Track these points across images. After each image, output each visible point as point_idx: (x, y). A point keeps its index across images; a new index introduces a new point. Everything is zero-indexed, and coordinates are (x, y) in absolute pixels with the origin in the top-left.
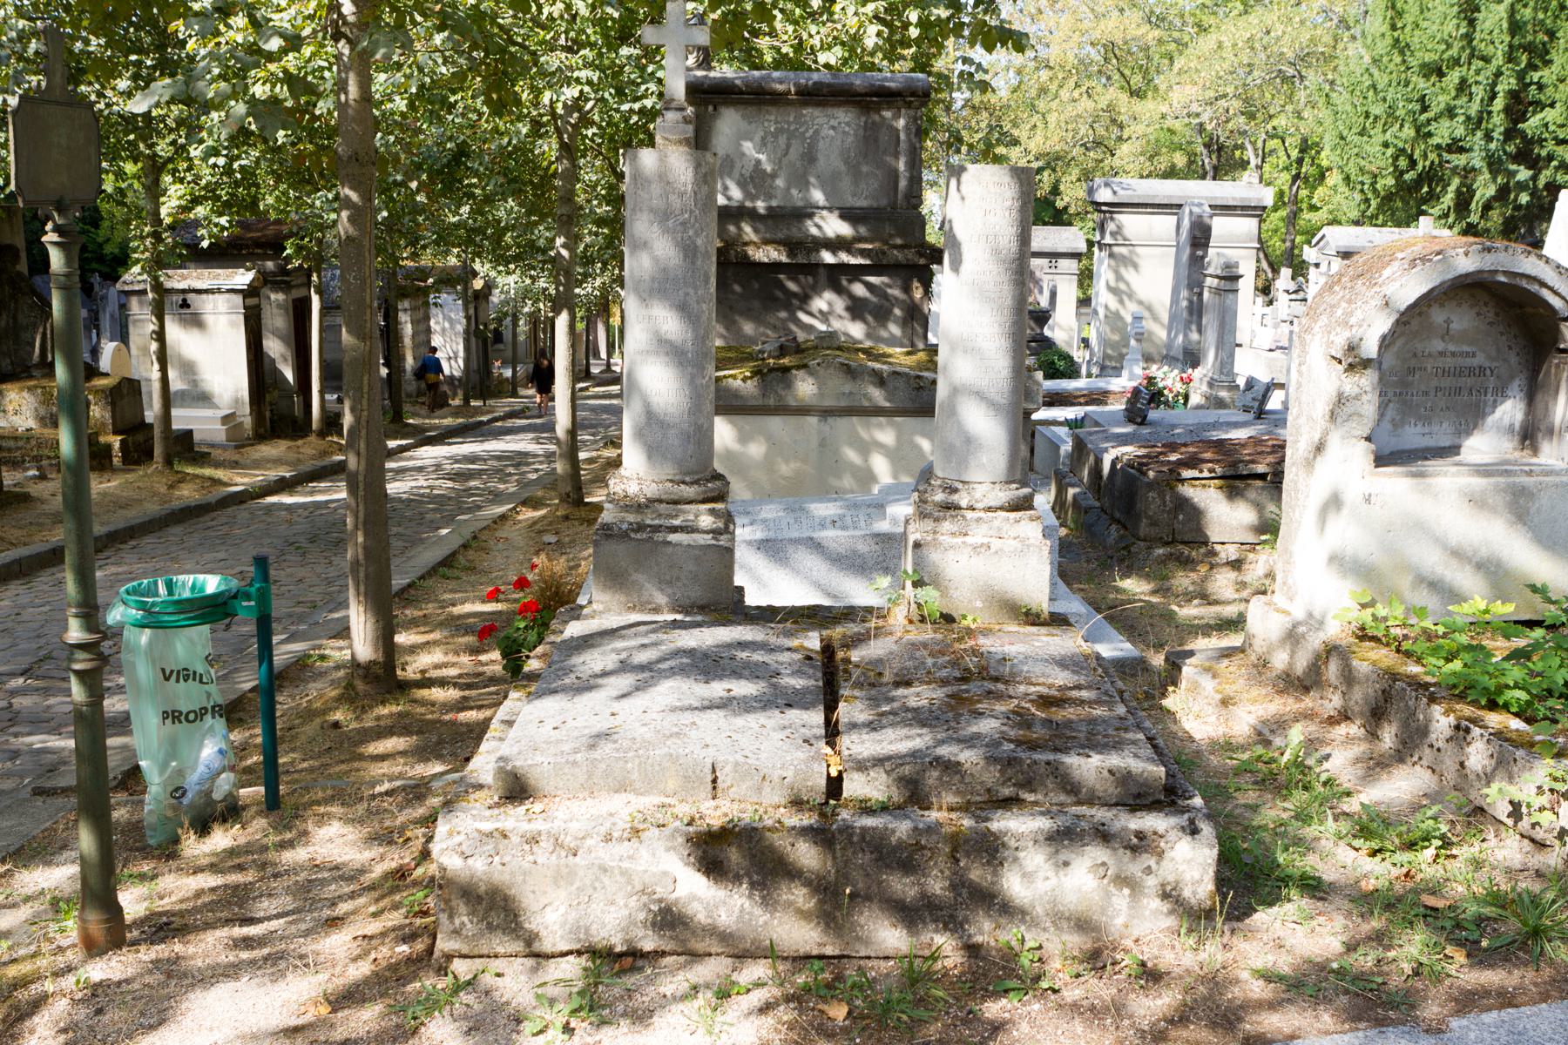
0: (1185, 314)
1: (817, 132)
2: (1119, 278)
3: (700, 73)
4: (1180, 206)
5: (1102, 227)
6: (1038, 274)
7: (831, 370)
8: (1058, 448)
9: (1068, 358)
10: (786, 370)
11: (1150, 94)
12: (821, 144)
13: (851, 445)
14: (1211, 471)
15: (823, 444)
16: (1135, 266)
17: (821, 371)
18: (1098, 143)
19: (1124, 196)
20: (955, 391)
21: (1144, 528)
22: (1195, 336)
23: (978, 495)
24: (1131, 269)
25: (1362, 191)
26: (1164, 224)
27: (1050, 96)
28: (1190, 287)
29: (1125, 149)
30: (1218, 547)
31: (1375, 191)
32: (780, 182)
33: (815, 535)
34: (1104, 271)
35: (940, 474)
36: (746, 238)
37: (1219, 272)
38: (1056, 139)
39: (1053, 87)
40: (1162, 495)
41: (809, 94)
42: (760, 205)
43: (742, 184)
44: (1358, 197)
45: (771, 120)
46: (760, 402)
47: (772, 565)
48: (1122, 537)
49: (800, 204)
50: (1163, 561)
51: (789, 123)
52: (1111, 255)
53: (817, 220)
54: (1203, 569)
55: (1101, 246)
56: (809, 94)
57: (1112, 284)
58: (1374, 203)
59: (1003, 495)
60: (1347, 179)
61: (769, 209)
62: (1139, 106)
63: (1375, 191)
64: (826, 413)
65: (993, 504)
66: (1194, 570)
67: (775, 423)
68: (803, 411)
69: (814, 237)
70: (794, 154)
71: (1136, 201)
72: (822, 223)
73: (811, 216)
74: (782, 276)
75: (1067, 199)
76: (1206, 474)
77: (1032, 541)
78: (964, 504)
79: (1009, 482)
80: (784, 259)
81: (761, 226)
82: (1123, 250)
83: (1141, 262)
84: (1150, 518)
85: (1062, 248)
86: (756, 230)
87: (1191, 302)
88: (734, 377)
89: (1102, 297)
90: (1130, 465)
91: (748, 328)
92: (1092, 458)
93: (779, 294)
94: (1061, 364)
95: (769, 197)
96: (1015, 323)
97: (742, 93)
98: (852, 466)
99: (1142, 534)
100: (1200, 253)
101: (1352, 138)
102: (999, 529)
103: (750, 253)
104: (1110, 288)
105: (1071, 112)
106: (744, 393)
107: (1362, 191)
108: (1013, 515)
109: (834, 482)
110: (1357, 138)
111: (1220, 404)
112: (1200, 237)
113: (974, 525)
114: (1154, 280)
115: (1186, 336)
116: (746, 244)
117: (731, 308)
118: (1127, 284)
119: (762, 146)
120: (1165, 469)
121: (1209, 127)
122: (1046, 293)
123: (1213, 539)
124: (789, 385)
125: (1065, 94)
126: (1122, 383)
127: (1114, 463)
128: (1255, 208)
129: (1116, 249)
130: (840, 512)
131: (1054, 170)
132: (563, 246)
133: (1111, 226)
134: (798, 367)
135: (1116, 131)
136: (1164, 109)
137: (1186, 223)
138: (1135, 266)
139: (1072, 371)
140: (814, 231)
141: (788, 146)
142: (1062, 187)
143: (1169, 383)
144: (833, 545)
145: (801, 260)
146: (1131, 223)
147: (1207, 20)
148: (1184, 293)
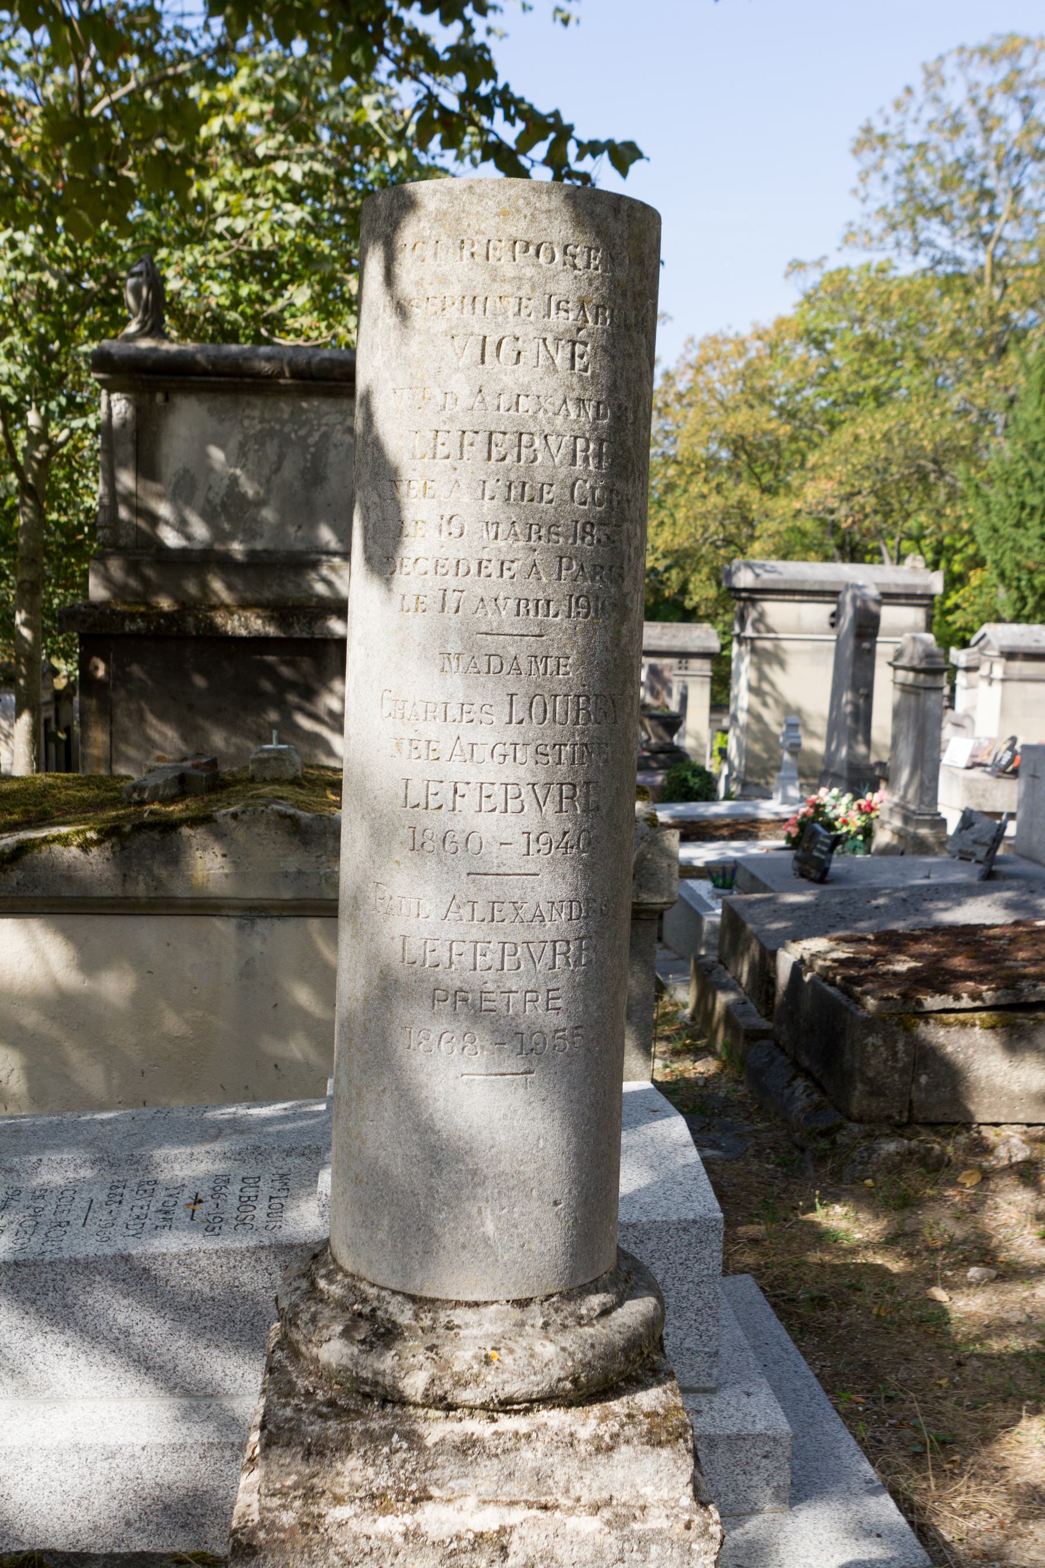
0: (849, 721)
1: (325, 436)
2: (762, 677)
3: (145, 344)
4: (835, 594)
5: (742, 620)
6: (666, 674)
7: (260, 829)
8: (699, 919)
9: (700, 772)
10: (169, 827)
11: (782, 491)
12: (332, 456)
13: (302, 976)
14: (975, 996)
15: (248, 971)
16: (782, 664)
17: (240, 834)
18: (728, 542)
19: (767, 579)
20: (388, 988)
21: (858, 1100)
22: (862, 749)
23: (463, 1357)
24: (776, 668)
25: (1018, 588)
26: (819, 613)
27: (678, 492)
28: (855, 688)
29: (757, 546)
30: (988, 1133)
31: (1033, 588)
32: (268, 514)
33: (135, 1250)
34: (744, 672)
35: (347, 1261)
36: (214, 600)
37: (916, 663)
38: (684, 535)
39: (682, 482)
40: (890, 1041)
41: (312, 378)
42: (237, 548)
43: (209, 517)
44: (1015, 595)
45: (255, 415)
46: (118, 891)
47: (29, 1323)
48: (818, 1108)
49: (300, 546)
50: (895, 1167)
51: (283, 423)
52: (754, 651)
53: (325, 571)
54: (969, 1180)
55: (741, 640)
56: (312, 378)
57: (754, 683)
58: (1031, 601)
59: (548, 1354)
60: (1002, 575)
61: (251, 554)
62: (769, 503)
63: (1033, 588)
64: (253, 912)
65: (516, 1388)
66: (953, 1183)
67: (148, 933)
68: (205, 907)
69: (320, 598)
70: (288, 471)
71: (782, 586)
72: (333, 577)
73: (315, 565)
74: (270, 658)
75: (696, 598)
76: (966, 1002)
77: (657, 1520)
78: (415, 1385)
79: (574, 1293)
80: (271, 630)
81: (239, 583)
82: (768, 645)
83: (791, 661)
84: (869, 1081)
85: (693, 646)
86: (230, 587)
87: (856, 706)
88: (65, 841)
89: (742, 697)
90: (825, 976)
91: (218, 739)
92: (754, 949)
93: (267, 685)
94: (694, 782)
95: (250, 534)
96: (588, 748)
97: (206, 373)
98: (305, 1014)
99: (855, 1110)
100: (866, 645)
101: (1006, 530)
102: (540, 1477)
103: (219, 620)
104: (751, 689)
105: (700, 507)
106: (86, 872)
107: (1018, 588)
108: (586, 1423)
109: (272, 1047)
110: (1010, 530)
111: (921, 847)
112: (867, 627)
113: (448, 1466)
114: (808, 683)
115: (850, 748)
116: (214, 608)
117: (190, 707)
118: (772, 685)
119: (241, 456)
120: (894, 994)
121: (844, 525)
122: (676, 696)
123: (979, 1119)
124: (175, 857)
125: (695, 489)
126: (779, 805)
127: (798, 968)
128: (922, 596)
129: (760, 644)
130: (220, 1167)
131: (683, 569)
132: (25, 624)
133: (752, 614)
134: (194, 822)
135: (746, 531)
136: (797, 505)
137: (849, 612)
138: (782, 664)
139: (708, 794)
140: (320, 588)
141: (281, 458)
142: (691, 587)
143: (841, 811)
144: (178, 1276)
145: (299, 632)
146: (778, 613)
147: (837, 414)
148: (847, 696)
